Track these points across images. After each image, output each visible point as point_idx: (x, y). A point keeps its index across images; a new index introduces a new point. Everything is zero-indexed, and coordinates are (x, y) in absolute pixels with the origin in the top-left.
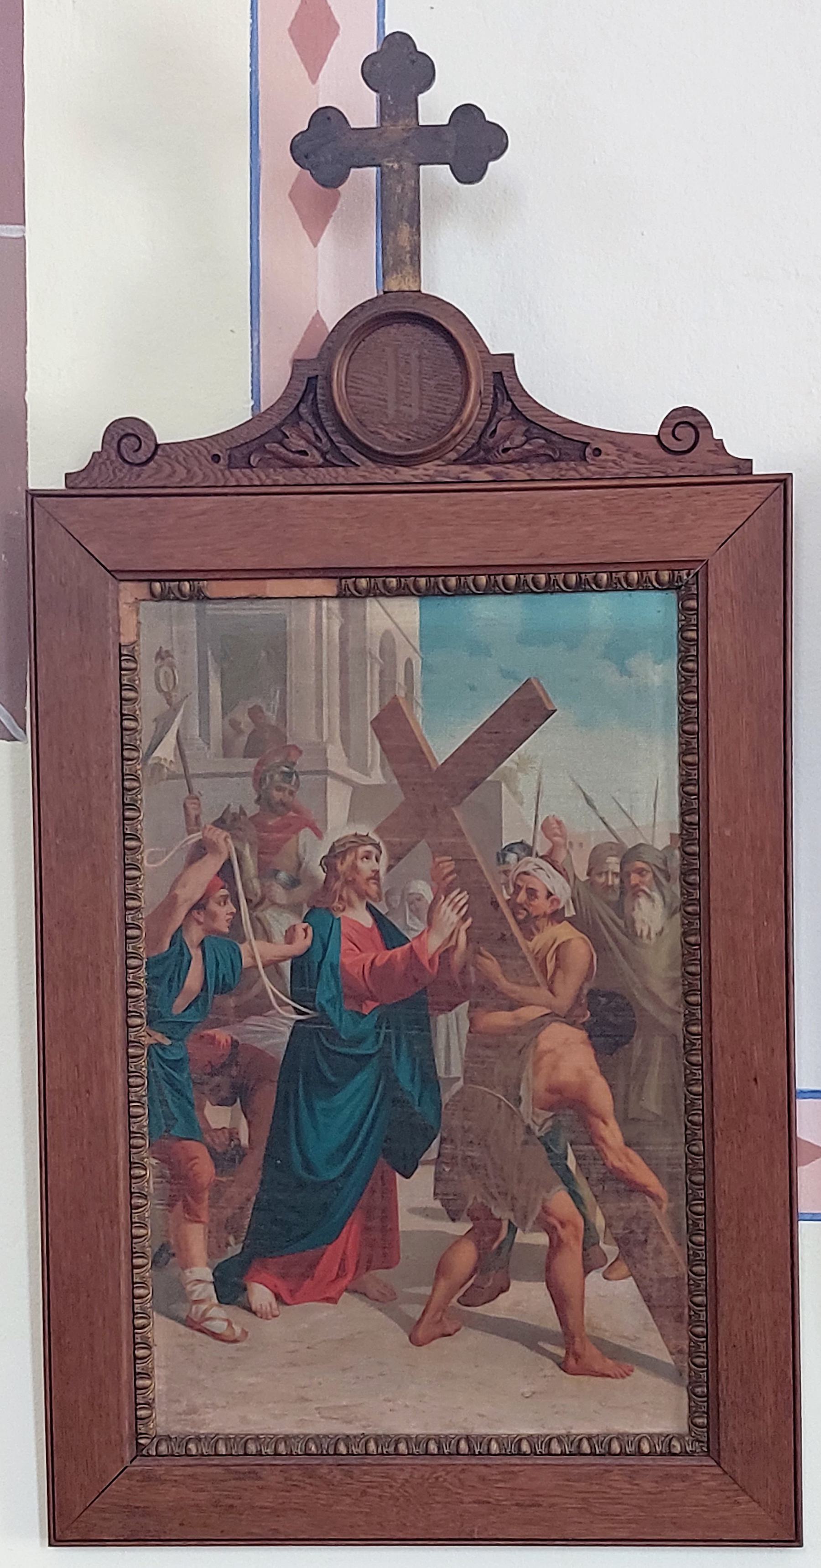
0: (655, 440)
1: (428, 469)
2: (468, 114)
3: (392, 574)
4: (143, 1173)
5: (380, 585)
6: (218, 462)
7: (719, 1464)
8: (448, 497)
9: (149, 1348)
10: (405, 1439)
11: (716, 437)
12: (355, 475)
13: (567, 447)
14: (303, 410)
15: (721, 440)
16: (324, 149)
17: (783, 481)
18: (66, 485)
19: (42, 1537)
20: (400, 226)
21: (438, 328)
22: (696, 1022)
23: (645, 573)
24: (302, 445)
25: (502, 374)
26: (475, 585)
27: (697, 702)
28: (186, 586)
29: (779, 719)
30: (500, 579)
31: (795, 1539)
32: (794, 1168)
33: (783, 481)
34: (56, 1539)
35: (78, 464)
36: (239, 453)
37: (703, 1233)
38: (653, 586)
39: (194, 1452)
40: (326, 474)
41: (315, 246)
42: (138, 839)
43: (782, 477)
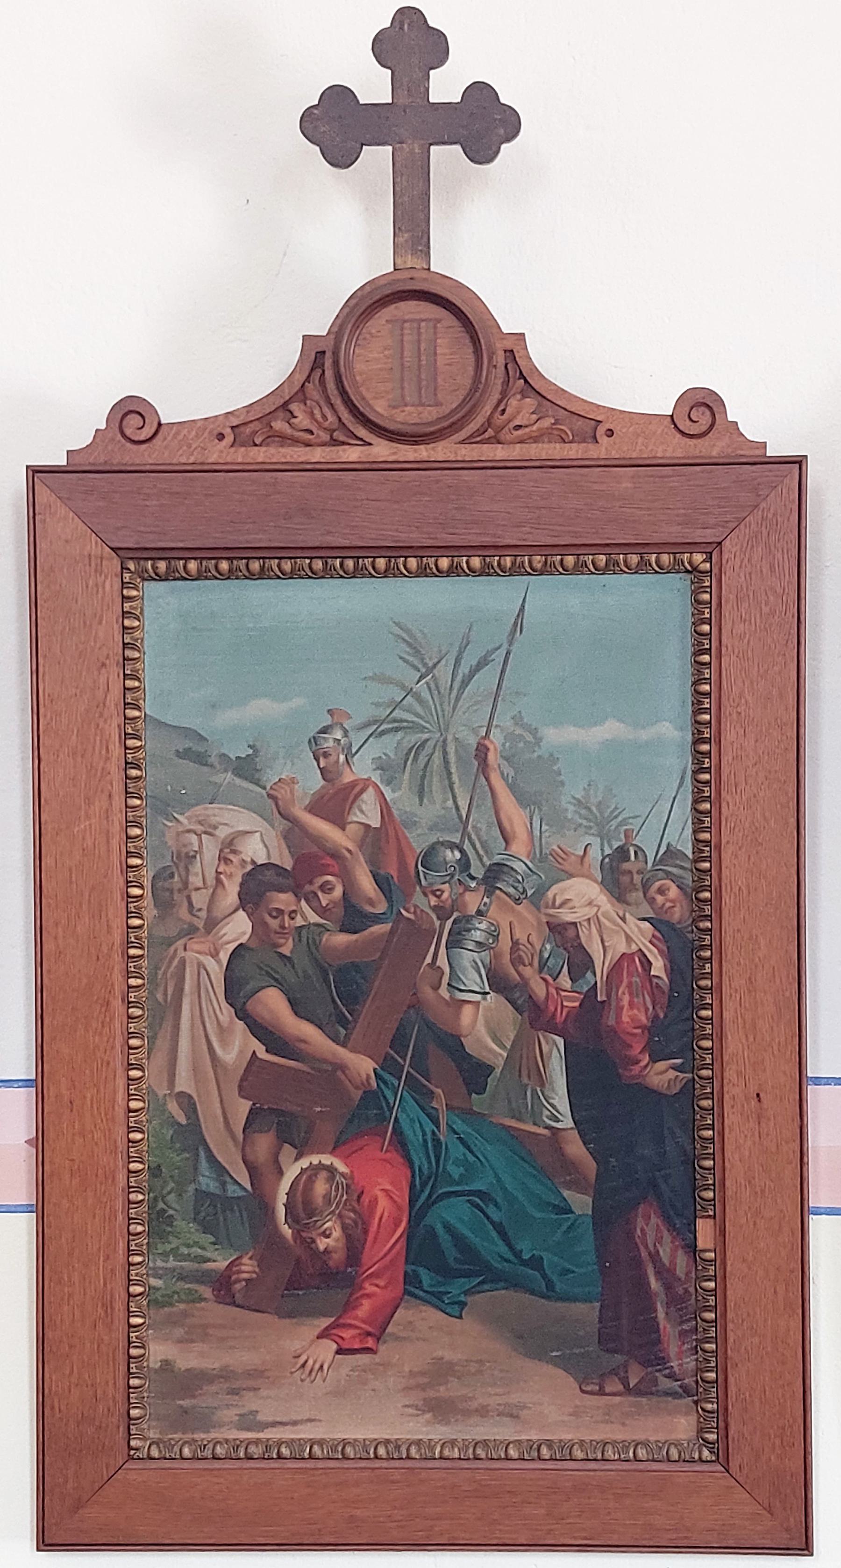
0: (669, 419)
1: (440, 451)
2: (481, 94)
3: (384, 554)
5: (243, 568)
7: (720, 543)
11: (730, 419)
12: (352, 454)
13: (587, 423)
15: (736, 423)
16: (336, 126)
19: (32, 1541)
20: (412, 222)
21: (456, 308)
23: (360, 560)
26: (374, 568)
28: (162, 566)
30: (653, 558)
31: (805, 1548)
33: (799, 462)
38: (653, 569)
39: (483, 1456)
43: (799, 459)
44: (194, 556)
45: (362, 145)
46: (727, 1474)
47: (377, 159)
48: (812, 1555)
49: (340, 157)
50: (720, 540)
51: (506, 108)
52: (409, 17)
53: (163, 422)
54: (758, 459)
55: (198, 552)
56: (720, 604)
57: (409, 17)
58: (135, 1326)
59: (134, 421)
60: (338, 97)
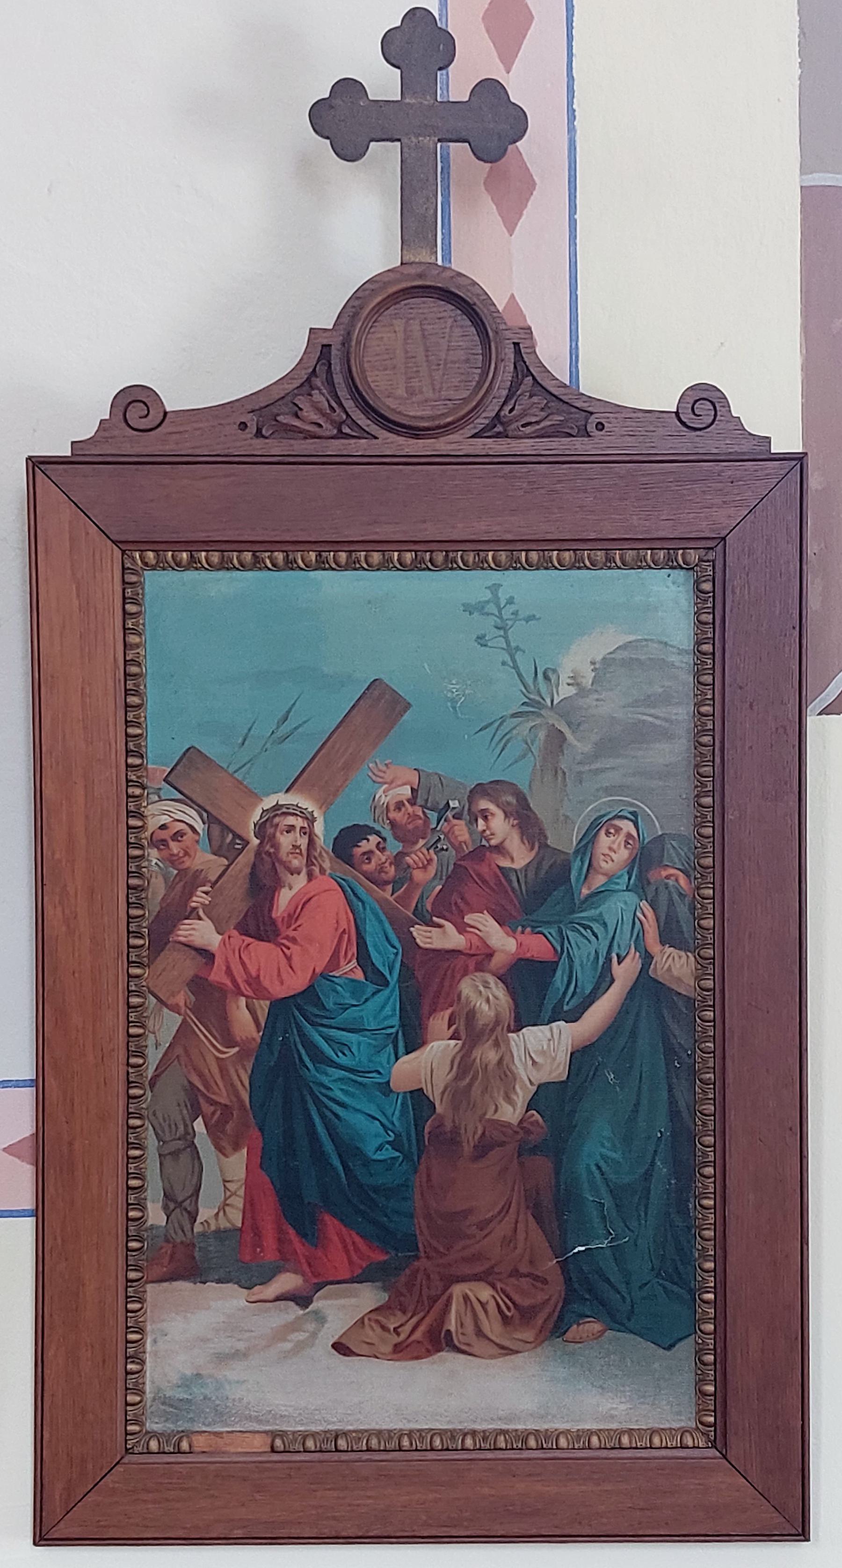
0: (674, 415)
2: (490, 90)
3: (534, 547)
6: (243, 430)
7: (724, 539)
8: (570, 468)
9: (142, 1362)
10: (313, 1435)
12: (360, 447)
13: (574, 413)
14: (317, 382)
16: (343, 120)
21: (466, 304)
24: (315, 417)
34: (35, 1544)
35: (87, 431)
36: (265, 412)
39: (690, 1444)
40: (336, 446)
41: (511, 232)
44: (151, 548)
46: (724, 1461)
47: (386, 157)
48: (808, 1540)
49: (349, 152)
51: (381, 104)
52: (416, 16)
53: (168, 409)
55: (385, 544)
58: (132, 1312)
59: (140, 409)
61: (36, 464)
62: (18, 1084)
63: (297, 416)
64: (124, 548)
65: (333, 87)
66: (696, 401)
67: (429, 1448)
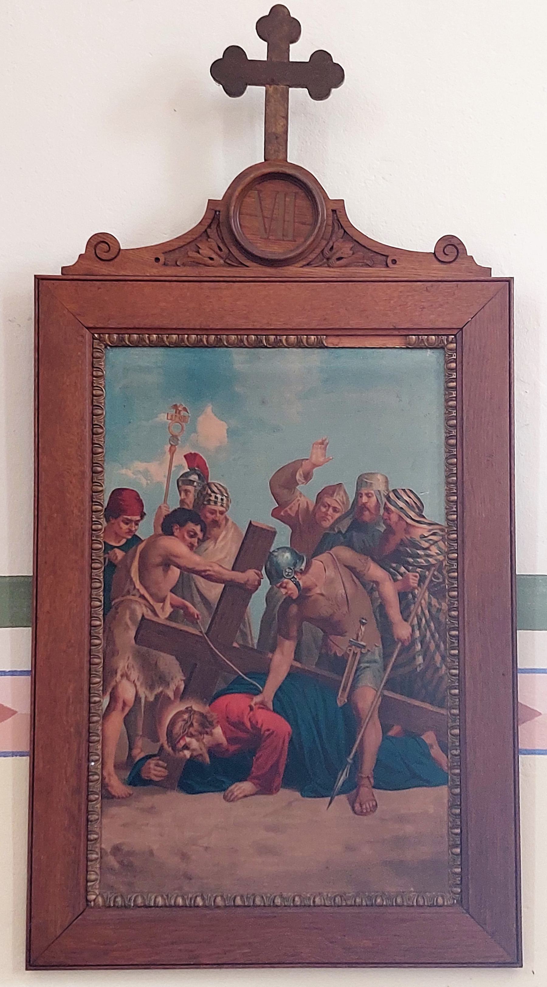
0: (433, 255)
2: (321, 57)
4: (101, 392)
7: (461, 329)
16: (232, 71)
17: (509, 281)
18: (62, 273)
21: (301, 184)
22: (456, 767)
25: (338, 209)
27: (458, 636)
29: (507, 572)
32: (514, 555)
33: (509, 281)
35: (71, 261)
37: (456, 589)
39: (201, 904)
42: (102, 467)
45: (247, 85)
47: (256, 94)
49: (234, 89)
50: (461, 327)
52: (278, 11)
53: (122, 248)
54: (483, 275)
56: (463, 541)
57: (278, 11)
59: (105, 246)
60: (234, 53)
61: (39, 279)
62: (22, 673)
63: (199, 253)
64: (92, 332)
65: (338, 64)
66: (445, 247)
67: (152, 904)
